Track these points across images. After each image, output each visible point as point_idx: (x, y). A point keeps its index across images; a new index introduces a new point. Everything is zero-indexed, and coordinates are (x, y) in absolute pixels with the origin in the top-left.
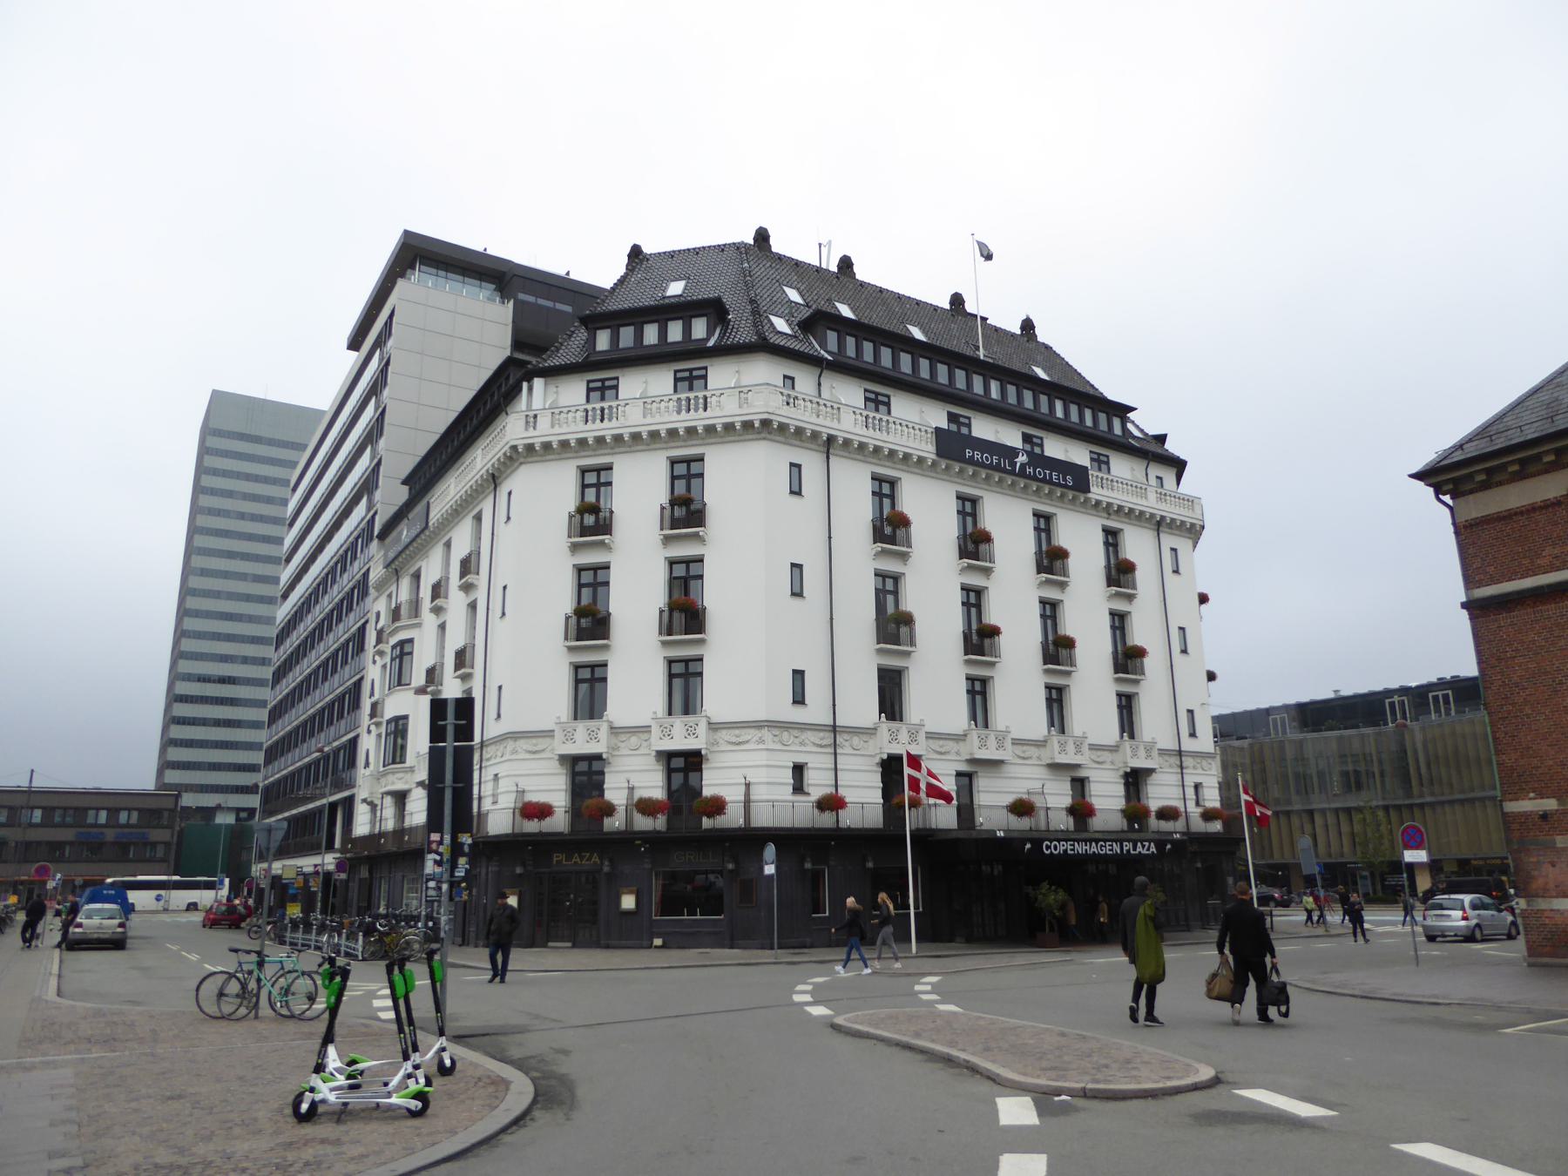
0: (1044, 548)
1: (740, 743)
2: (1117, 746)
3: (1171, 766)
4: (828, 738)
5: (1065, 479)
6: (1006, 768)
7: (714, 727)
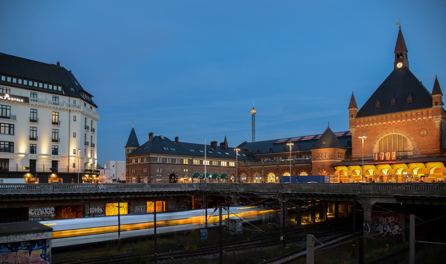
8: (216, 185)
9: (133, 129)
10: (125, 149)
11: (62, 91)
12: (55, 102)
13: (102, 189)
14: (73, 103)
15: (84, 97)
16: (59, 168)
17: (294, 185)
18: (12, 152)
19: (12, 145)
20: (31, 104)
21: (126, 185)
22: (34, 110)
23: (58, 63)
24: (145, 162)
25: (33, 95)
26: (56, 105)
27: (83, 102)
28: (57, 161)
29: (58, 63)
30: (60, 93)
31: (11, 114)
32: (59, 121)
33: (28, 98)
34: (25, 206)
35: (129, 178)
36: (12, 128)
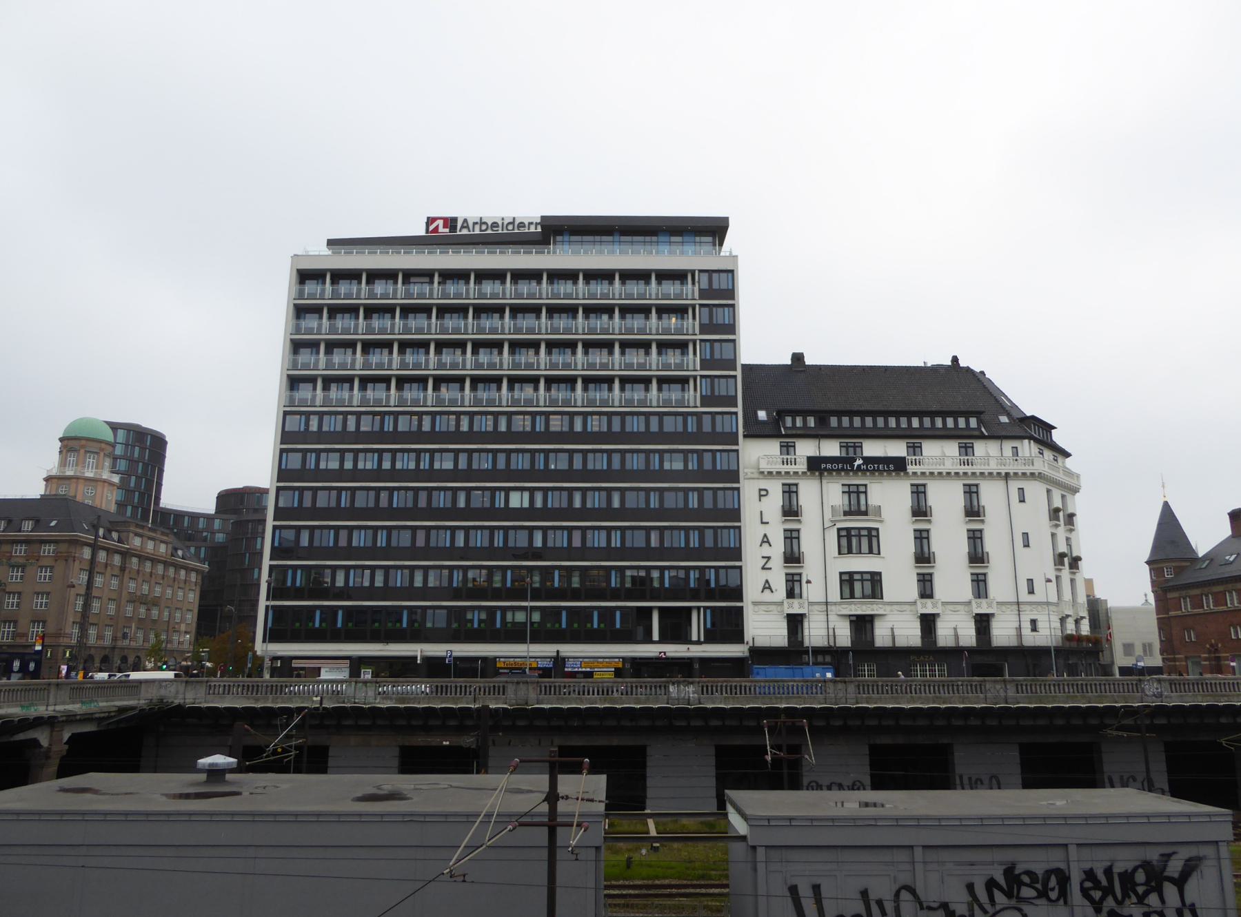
0: (283, 467)
1: (770, 611)
2: (1058, 603)
3: (1012, 611)
4: (824, 607)
5: (888, 467)
6: (886, 617)
7: (811, 604)
8: (85, 686)
9: (1166, 505)
10: (1147, 567)
11: (979, 429)
12: (787, 459)
13: (1154, 695)
14: (958, 454)
15: (1035, 433)
16: (994, 634)
17: (1215, 683)
18: (880, 597)
19: (877, 581)
20: (911, 474)
21: (1231, 682)
22: (849, 485)
23: (955, 359)
24: (1232, 603)
25: (912, 449)
26: (789, 464)
27: (1035, 448)
28: (934, 615)
29: (955, 359)
30: (976, 433)
31: (869, 503)
32: (928, 506)
33: (905, 458)
34: (945, 741)
35: (1174, 660)
36: (875, 536)
